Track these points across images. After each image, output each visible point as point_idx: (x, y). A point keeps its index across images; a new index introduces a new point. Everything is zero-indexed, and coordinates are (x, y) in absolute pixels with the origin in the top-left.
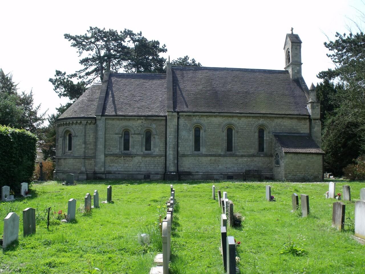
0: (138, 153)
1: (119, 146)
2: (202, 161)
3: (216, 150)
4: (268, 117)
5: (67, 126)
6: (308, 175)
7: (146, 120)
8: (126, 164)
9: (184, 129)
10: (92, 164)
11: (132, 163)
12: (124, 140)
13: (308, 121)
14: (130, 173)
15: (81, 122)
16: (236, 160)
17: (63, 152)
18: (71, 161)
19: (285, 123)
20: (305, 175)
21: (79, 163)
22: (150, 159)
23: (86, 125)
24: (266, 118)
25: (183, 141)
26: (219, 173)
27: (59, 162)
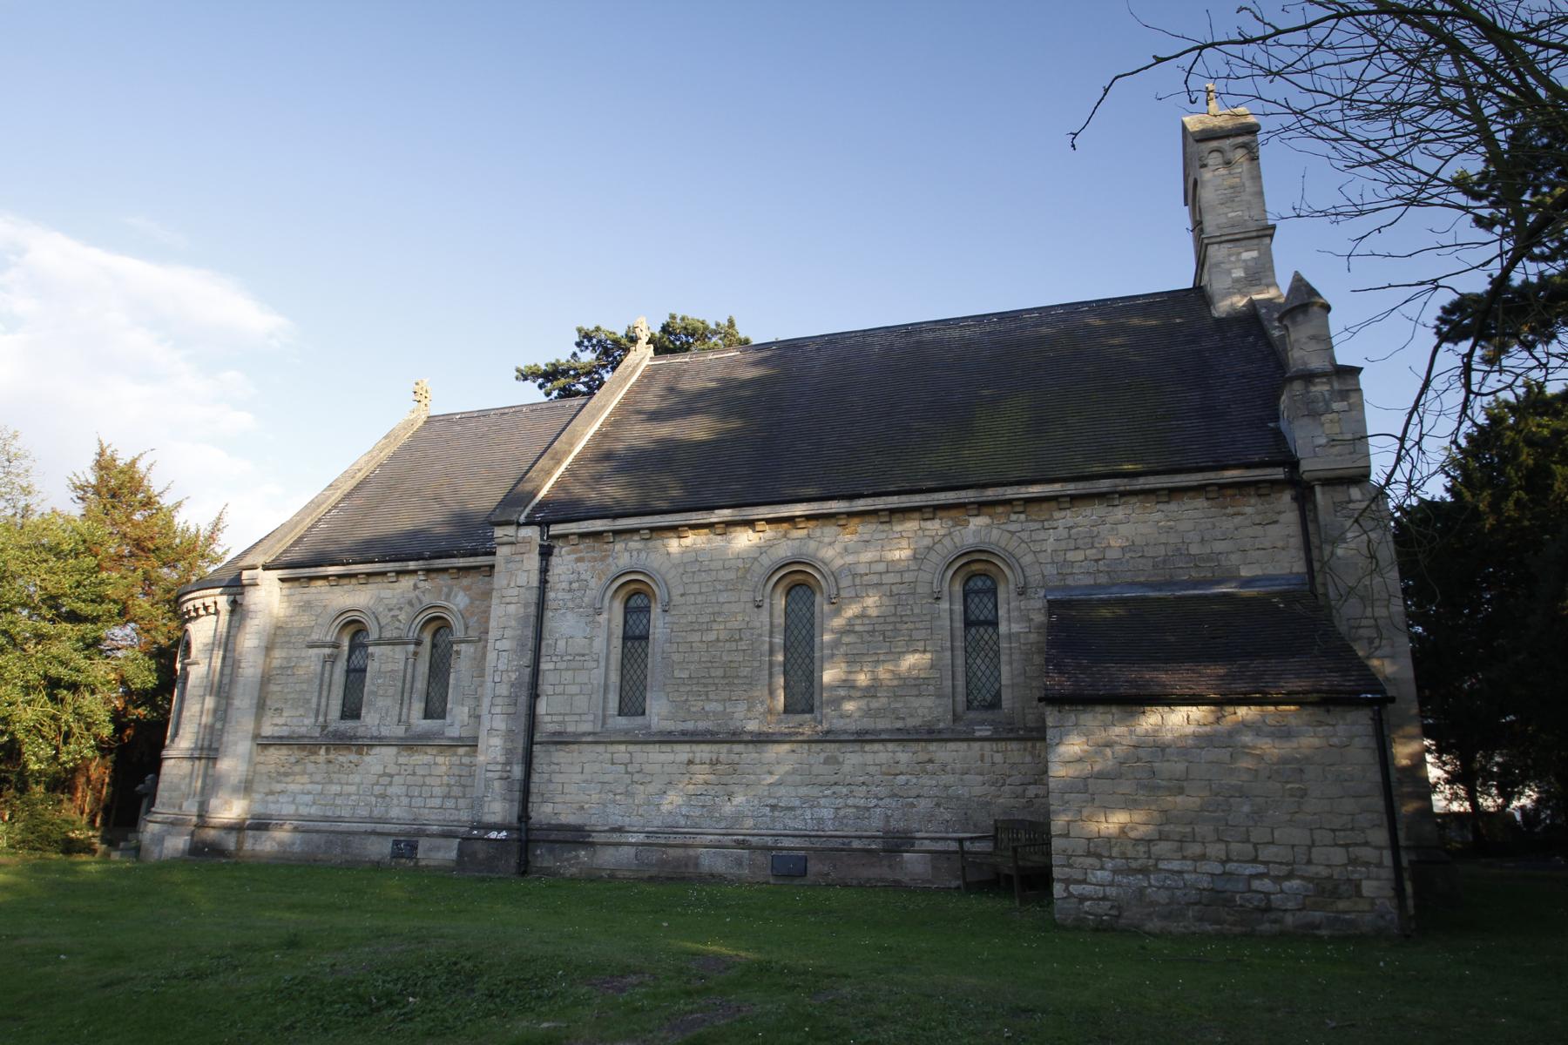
0: (385, 732)
1: (314, 700)
2: (647, 768)
3: (720, 708)
4: (1009, 502)
6: (1261, 869)
7: (433, 575)
8: (331, 782)
9: (570, 604)
11: (357, 779)
13: (1286, 497)
14: (344, 826)
16: (826, 762)
20: (1230, 867)
22: (426, 759)
24: (1000, 509)
25: (563, 666)
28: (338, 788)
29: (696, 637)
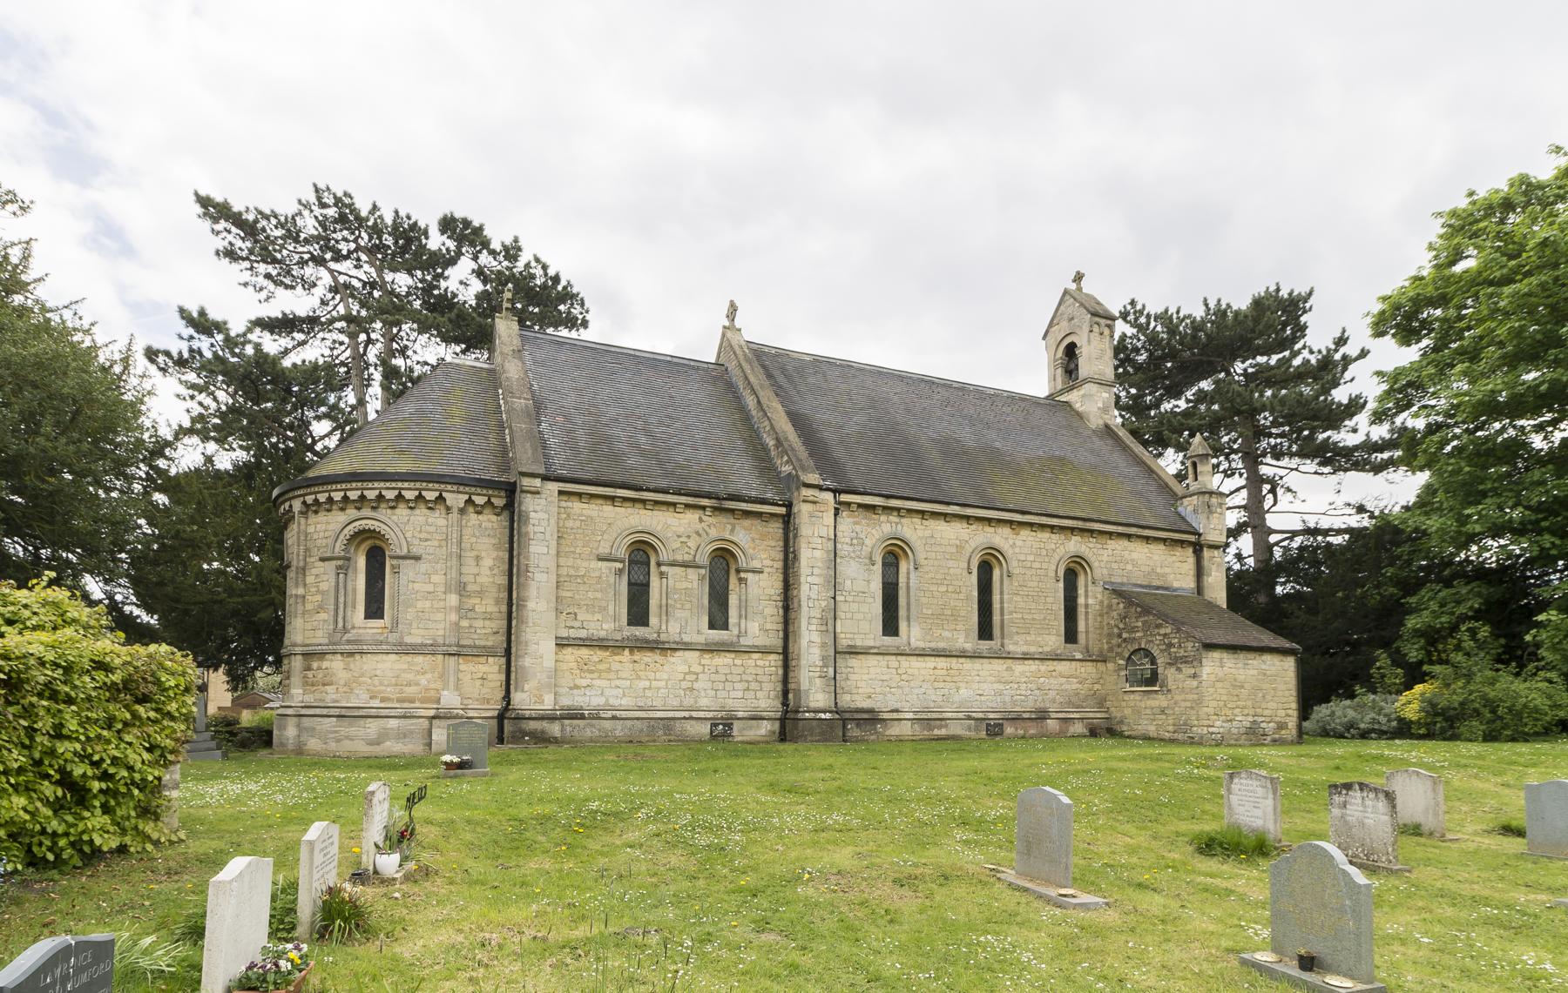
0: (686, 638)
1: (611, 608)
5: (366, 512)
10: (490, 677)
11: (665, 676)
12: (630, 584)
15: (441, 499)
17: (340, 625)
18: (387, 666)
21: (429, 676)
23: (462, 511)
26: (961, 715)
27: (309, 669)
28: (647, 684)
29: (934, 588)
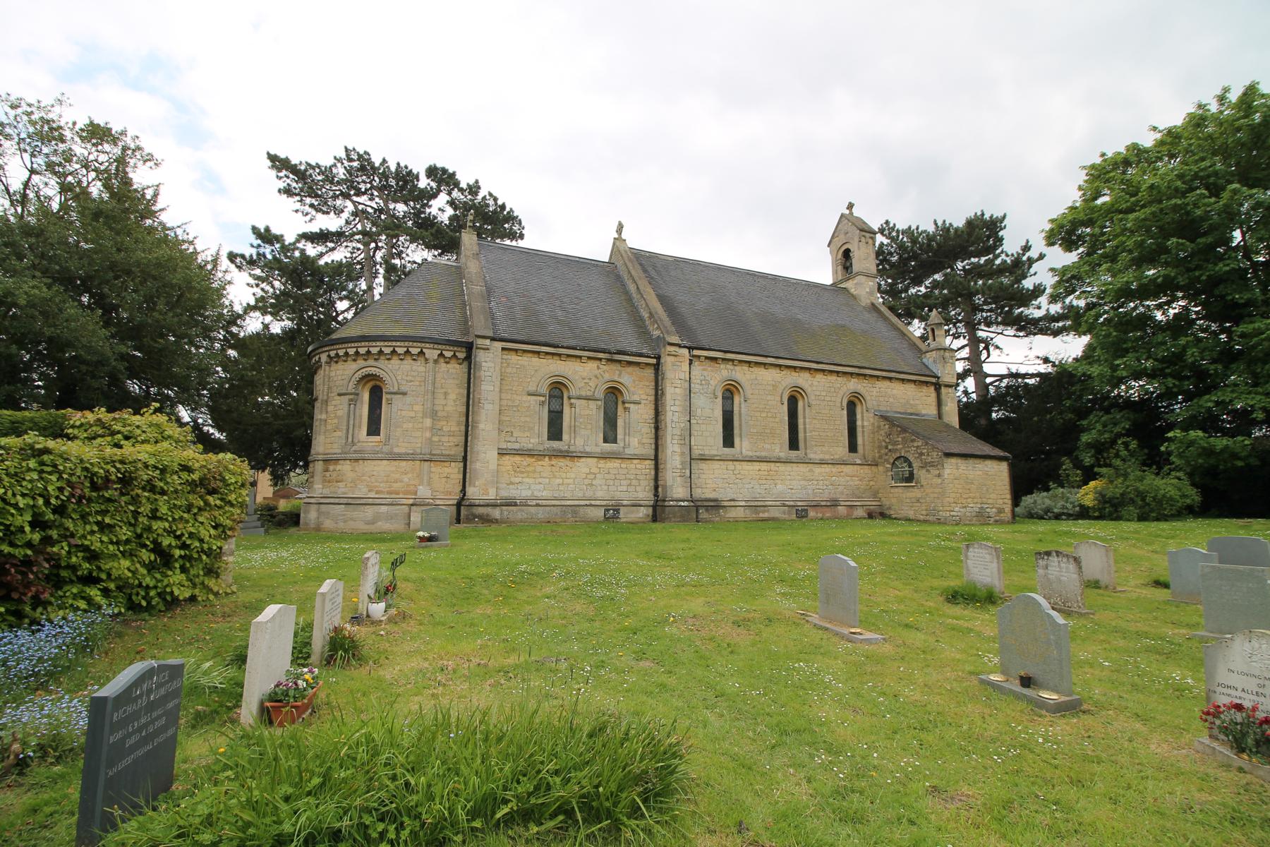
0: (588, 449)
8: (555, 477)
11: (573, 476)
15: (422, 353)
19: (895, 392)
